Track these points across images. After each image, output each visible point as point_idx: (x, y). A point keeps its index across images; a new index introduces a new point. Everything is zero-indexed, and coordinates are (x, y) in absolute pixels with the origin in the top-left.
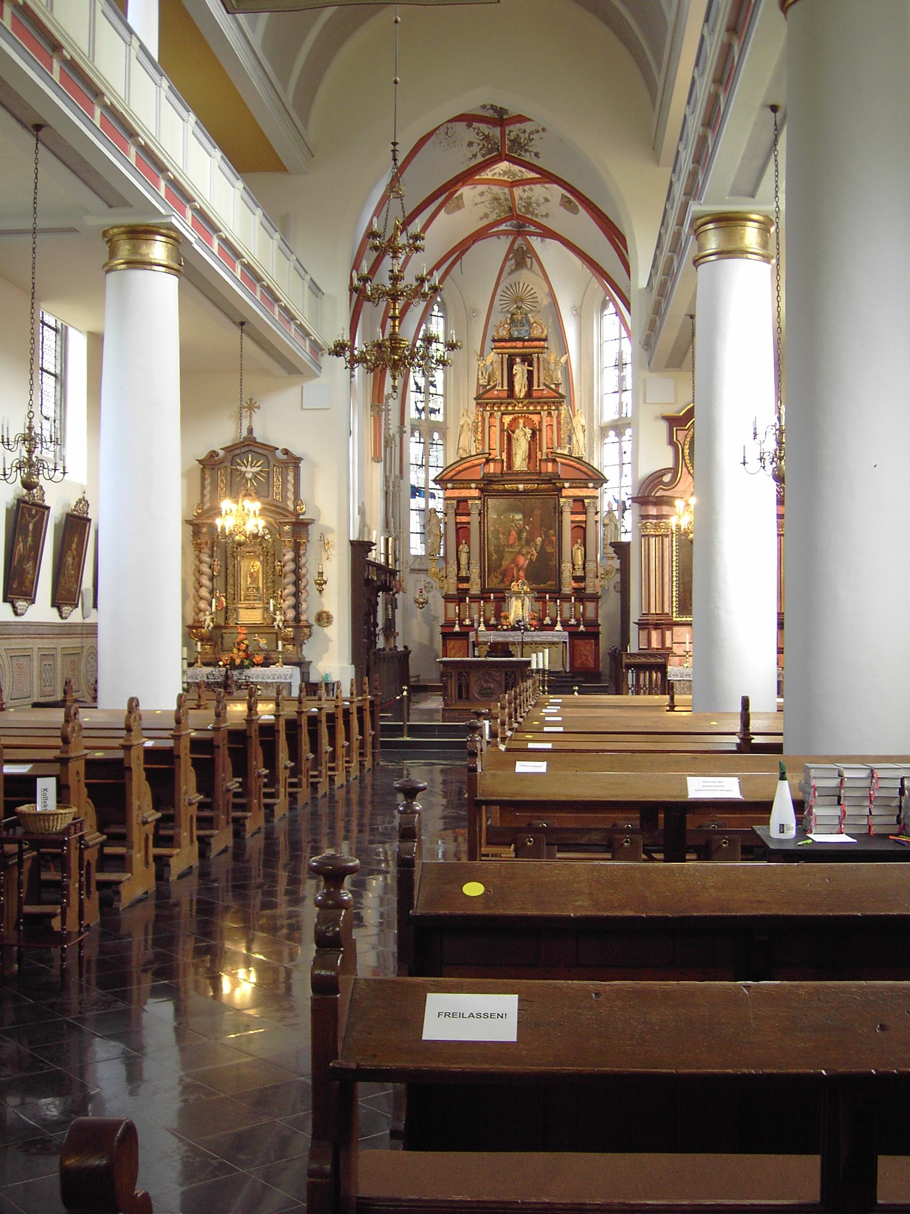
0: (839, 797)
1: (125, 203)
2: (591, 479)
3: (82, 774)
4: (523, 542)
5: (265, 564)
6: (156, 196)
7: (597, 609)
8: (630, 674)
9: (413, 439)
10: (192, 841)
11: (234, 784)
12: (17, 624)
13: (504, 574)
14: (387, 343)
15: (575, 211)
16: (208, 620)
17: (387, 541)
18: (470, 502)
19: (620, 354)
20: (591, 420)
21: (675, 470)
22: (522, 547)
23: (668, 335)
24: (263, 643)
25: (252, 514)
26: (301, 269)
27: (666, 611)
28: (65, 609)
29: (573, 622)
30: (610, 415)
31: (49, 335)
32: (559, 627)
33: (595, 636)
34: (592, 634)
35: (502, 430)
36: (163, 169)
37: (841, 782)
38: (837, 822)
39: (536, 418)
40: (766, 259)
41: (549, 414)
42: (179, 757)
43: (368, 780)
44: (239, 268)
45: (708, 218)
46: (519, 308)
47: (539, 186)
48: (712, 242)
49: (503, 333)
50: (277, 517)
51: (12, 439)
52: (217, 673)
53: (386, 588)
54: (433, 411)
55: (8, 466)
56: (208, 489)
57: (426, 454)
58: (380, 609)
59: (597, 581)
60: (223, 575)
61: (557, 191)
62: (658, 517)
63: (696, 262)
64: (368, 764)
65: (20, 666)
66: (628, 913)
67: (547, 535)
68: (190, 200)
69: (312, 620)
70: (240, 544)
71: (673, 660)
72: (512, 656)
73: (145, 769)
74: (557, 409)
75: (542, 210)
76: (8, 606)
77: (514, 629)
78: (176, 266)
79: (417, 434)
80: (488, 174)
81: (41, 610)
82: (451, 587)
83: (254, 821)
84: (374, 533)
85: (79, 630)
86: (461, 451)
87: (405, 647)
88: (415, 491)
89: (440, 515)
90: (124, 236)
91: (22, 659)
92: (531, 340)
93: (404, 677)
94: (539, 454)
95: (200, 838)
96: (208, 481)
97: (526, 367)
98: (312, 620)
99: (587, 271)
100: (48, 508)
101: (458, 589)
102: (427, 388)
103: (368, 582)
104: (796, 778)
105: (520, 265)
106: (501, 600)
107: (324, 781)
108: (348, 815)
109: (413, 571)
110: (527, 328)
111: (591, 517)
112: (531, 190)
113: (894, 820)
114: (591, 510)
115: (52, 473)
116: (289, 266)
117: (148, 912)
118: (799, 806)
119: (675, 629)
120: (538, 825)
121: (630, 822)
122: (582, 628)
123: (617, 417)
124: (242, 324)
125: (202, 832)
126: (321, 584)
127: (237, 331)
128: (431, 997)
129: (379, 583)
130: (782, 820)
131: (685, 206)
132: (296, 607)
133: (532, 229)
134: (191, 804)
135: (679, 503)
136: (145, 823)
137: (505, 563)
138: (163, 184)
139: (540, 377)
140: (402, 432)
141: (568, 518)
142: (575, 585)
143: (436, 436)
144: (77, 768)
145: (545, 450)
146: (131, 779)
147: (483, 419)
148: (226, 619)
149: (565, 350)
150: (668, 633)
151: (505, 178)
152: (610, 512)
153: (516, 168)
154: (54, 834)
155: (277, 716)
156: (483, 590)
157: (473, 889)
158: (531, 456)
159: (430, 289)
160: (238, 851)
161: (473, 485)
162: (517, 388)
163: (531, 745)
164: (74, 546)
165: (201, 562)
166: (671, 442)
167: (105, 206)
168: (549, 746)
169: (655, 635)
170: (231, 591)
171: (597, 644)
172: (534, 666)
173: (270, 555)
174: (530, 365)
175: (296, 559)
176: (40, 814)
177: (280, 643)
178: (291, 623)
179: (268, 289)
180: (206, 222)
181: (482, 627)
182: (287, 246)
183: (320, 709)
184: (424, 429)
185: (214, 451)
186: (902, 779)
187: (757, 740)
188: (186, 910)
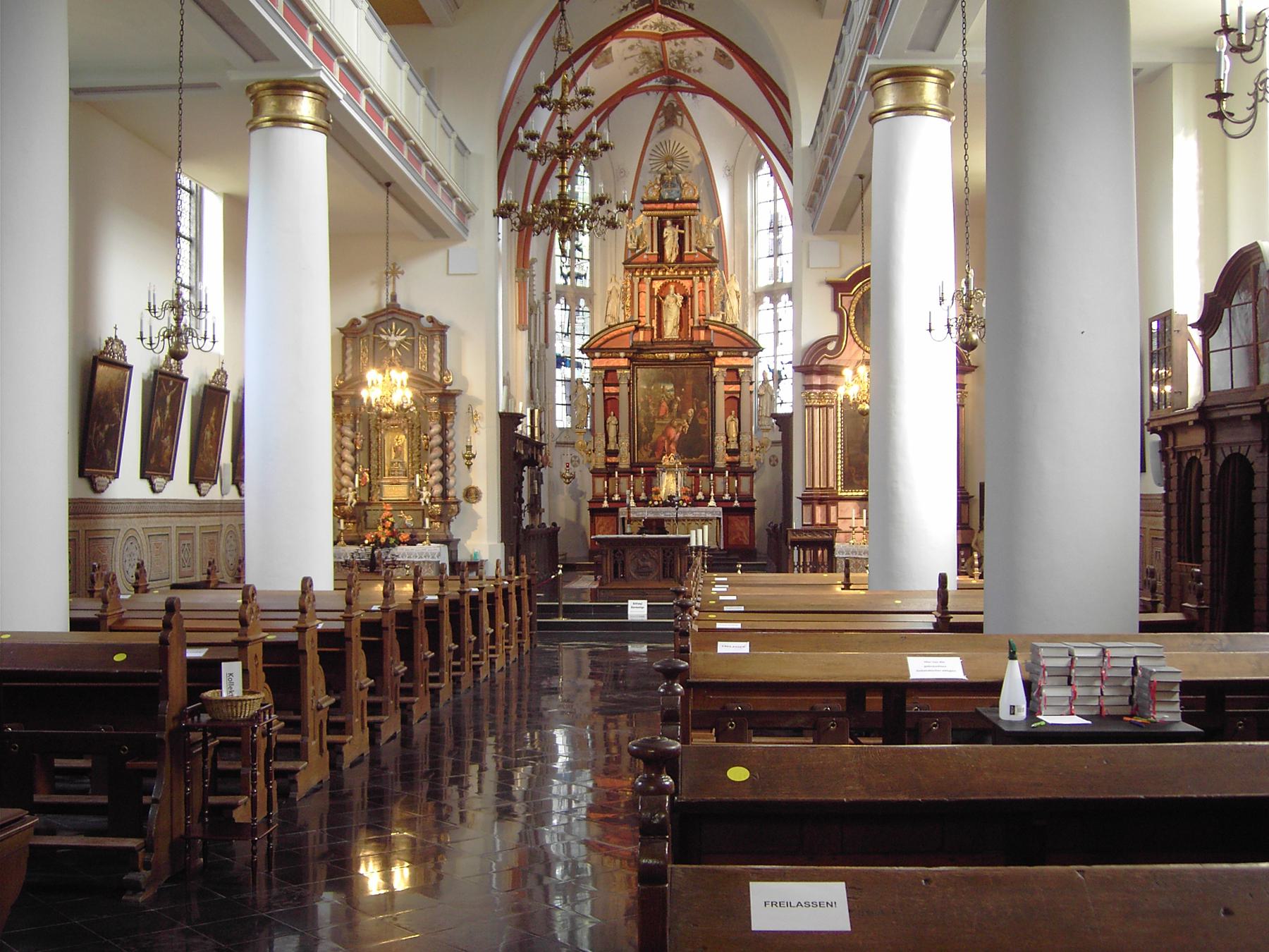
0: (1070, 678)
1: (271, 57)
2: (746, 348)
3: (260, 660)
4: (675, 414)
5: (410, 437)
6: (303, 49)
7: (752, 483)
8: (796, 552)
9: (558, 306)
10: (363, 728)
11: (401, 668)
12: (154, 501)
13: (655, 447)
14: (557, 204)
15: (729, 65)
16: (350, 496)
17: (532, 412)
18: (618, 372)
19: (776, 216)
20: (744, 285)
21: (839, 338)
22: (673, 418)
23: (836, 195)
24: (409, 520)
25: (399, 385)
26: (447, 127)
27: (831, 485)
28: (204, 485)
29: (727, 497)
30: (764, 281)
31: (185, 196)
32: (712, 503)
33: (750, 511)
34: (747, 510)
35: (652, 297)
36: (311, 21)
37: (1072, 661)
38: (1067, 703)
39: (687, 284)
40: (946, 116)
41: (702, 279)
42: (350, 639)
43: (526, 664)
44: (386, 125)
45: (885, 73)
46: (670, 168)
47: (692, 39)
48: (890, 99)
49: (653, 194)
50: (422, 387)
51: (159, 306)
52: (363, 552)
53: (532, 462)
54: (579, 276)
55: (155, 334)
56: (350, 358)
57: (572, 321)
58: (525, 484)
59: (752, 454)
60: (366, 448)
61: (711, 44)
62: (822, 387)
63: (873, 119)
64: (526, 647)
65: (157, 546)
66: (902, 797)
67: (699, 406)
68: (337, 53)
69: (460, 497)
70: (388, 417)
71: (840, 536)
72: (666, 533)
73: (319, 653)
74: (710, 274)
75: (695, 65)
76: (145, 483)
77: (665, 504)
78: (324, 123)
79: (562, 301)
80: (638, 27)
81: (179, 487)
82: (599, 460)
83: (421, 706)
84: (521, 405)
85: (217, 508)
86: (609, 318)
87: (554, 524)
88: (561, 361)
89: (587, 386)
90: (269, 92)
91: (160, 539)
92: (682, 201)
93: (552, 556)
94: (691, 321)
95: (370, 725)
96: (349, 351)
97: (677, 230)
98: (460, 497)
99: (741, 129)
100: (186, 380)
101: (607, 463)
102: (572, 252)
103: (517, 456)
104: (1024, 656)
105: (670, 122)
106: (652, 476)
107: (485, 663)
108: (507, 699)
109: (559, 444)
110: (678, 188)
111: (746, 388)
112: (684, 43)
113: (1126, 700)
114: (746, 380)
115: (201, 342)
116: (436, 124)
117: (321, 803)
118: (1028, 687)
119: (840, 503)
120: (738, 708)
121: (835, 703)
122: (736, 503)
123: (772, 282)
124: (388, 184)
125: (372, 719)
126: (469, 459)
127: (382, 192)
128: (755, 887)
129: (526, 457)
130: (1012, 703)
131: (859, 61)
132: (443, 482)
133: (684, 84)
134: (361, 689)
135: (847, 373)
136: (319, 709)
137: (655, 436)
138: (310, 36)
139: (692, 241)
140: (547, 299)
141: (721, 389)
142: (728, 458)
143: (582, 303)
144: (255, 650)
145: (697, 317)
146: (306, 663)
147: (632, 282)
148: (370, 495)
149: (718, 213)
150: (833, 509)
151: (657, 31)
152: (765, 382)
153: (669, 20)
154: (243, 721)
155: (441, 597)
156: (632, 464)
157: (738, 774)
158: (682, 323)
159: (600, 147)
160: (406, 738)
161: (622, 354)
162: (668, 252)
163: (719, 625)
164: (212, 419)
165: (343, 435)
166: (836, 309)
167: (248, 60)
168: (738, 626)
169: (819, 510)
170: (374, 465)
171: (752, 521)
172: (693, 543)
173: (415, 427)
174: (682, 228)
175: (443, 433)
176: (227, 701)
177: (427, 520)
178: (438, 500)
179: (416, 148)
180: (352, 76)
181: (632, 504)
182: (433, 104)
183: (481, 589)
184: (570, 295)
185: (355, 320)
186: (1135, 658)
187: (955, 619)
188: (358, 798)
